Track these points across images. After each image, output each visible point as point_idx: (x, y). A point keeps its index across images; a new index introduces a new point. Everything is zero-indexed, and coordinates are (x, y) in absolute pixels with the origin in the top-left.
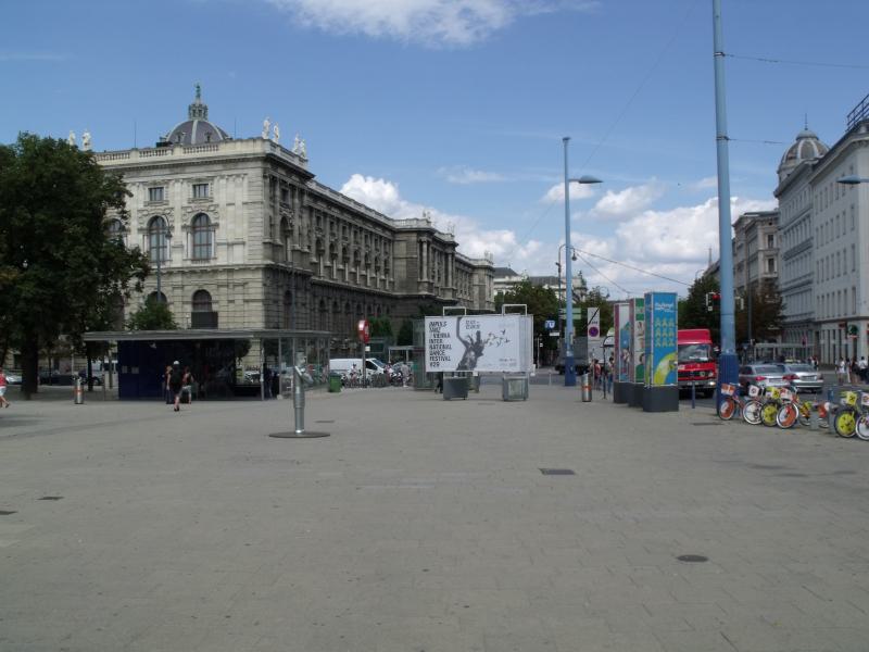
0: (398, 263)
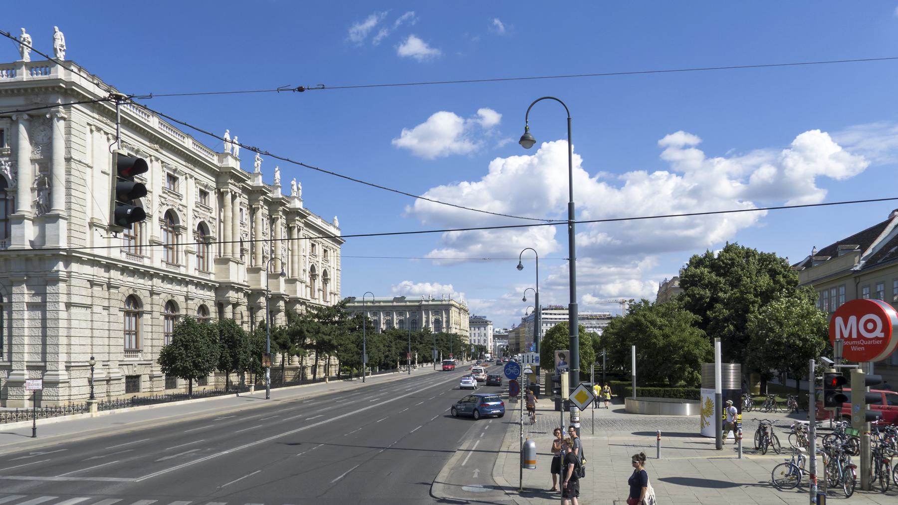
0: (238, 315)
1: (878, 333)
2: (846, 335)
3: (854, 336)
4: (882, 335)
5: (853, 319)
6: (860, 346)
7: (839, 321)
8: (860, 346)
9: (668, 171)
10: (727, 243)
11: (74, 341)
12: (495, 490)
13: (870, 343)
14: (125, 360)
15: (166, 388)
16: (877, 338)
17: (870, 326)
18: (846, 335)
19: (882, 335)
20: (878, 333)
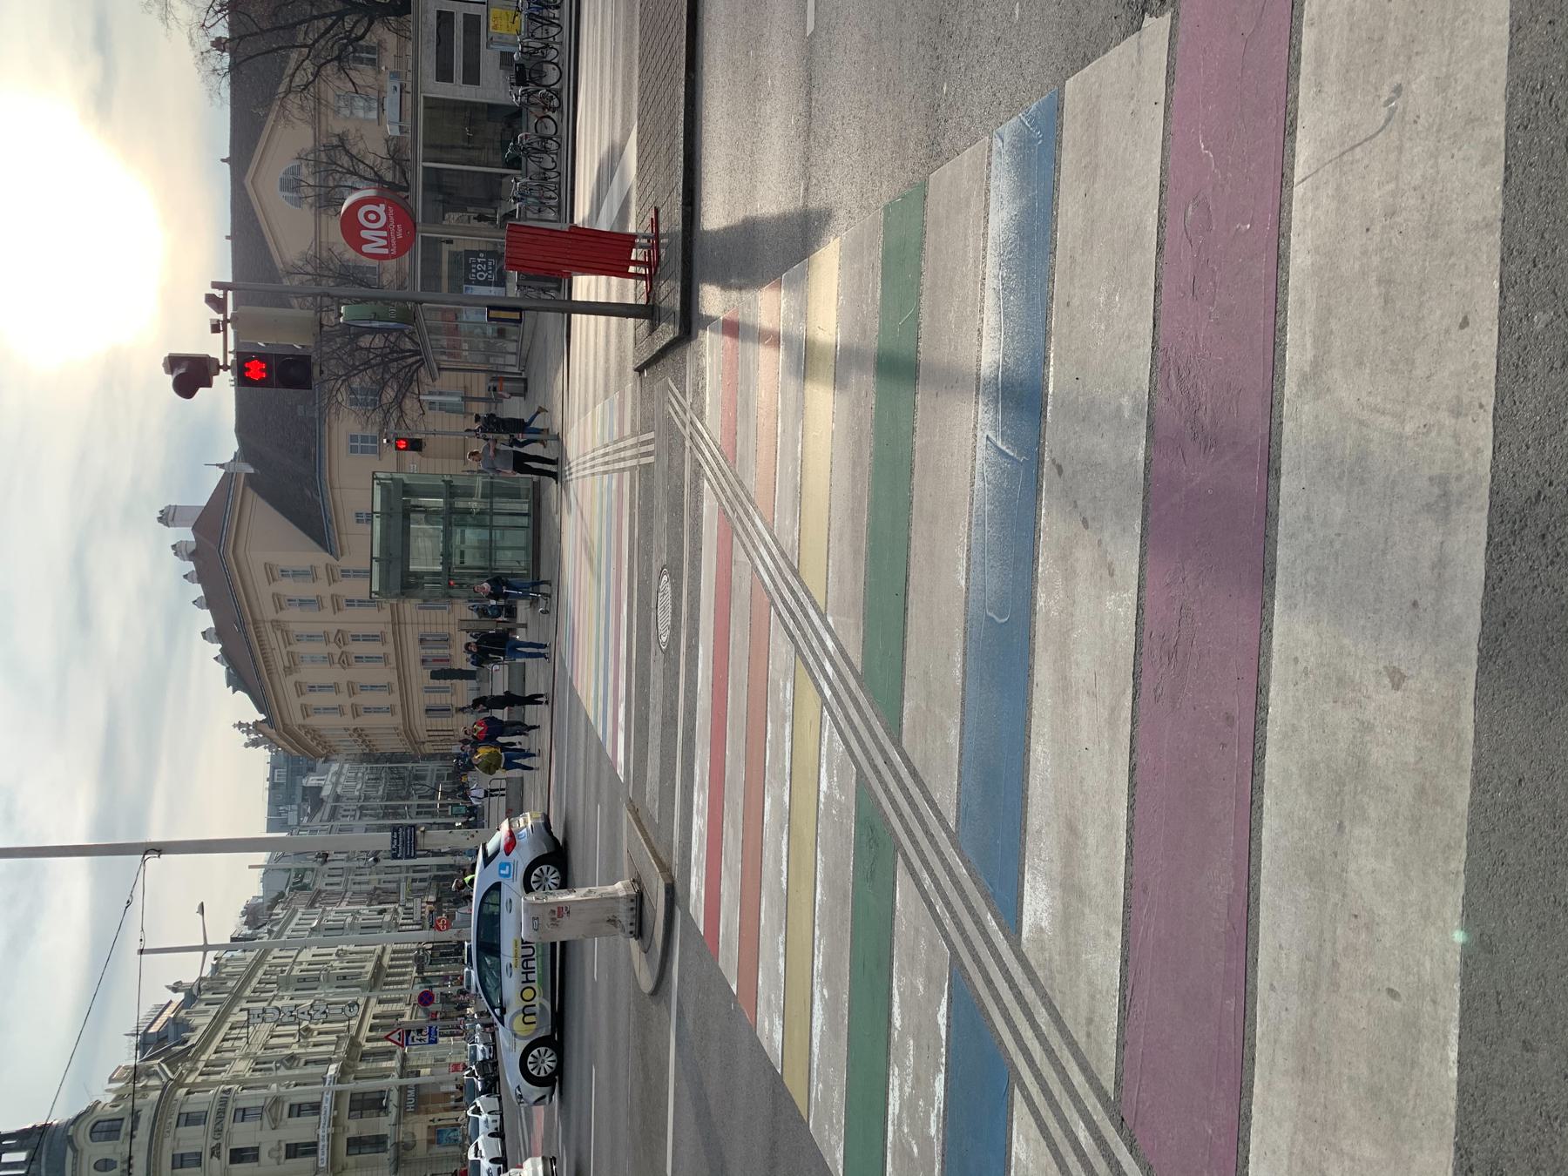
1: (381, 209)
2: (384, 242)
3: (384, 234)
4: (383, 206)
5: (364, 234)
6: (396, 229)
7: (366, 248)
8: (396, 229)
9: (498, 697)
10: (223, 160)
11: (589, 479)
12: (40, 1122)
13: (392, 219)
14: (394, 665)
15: (465, 15)
16: (386, 211)
17: (371, 216)
18: (384, 242)
19: (383, 206)
20: (381, 209)
